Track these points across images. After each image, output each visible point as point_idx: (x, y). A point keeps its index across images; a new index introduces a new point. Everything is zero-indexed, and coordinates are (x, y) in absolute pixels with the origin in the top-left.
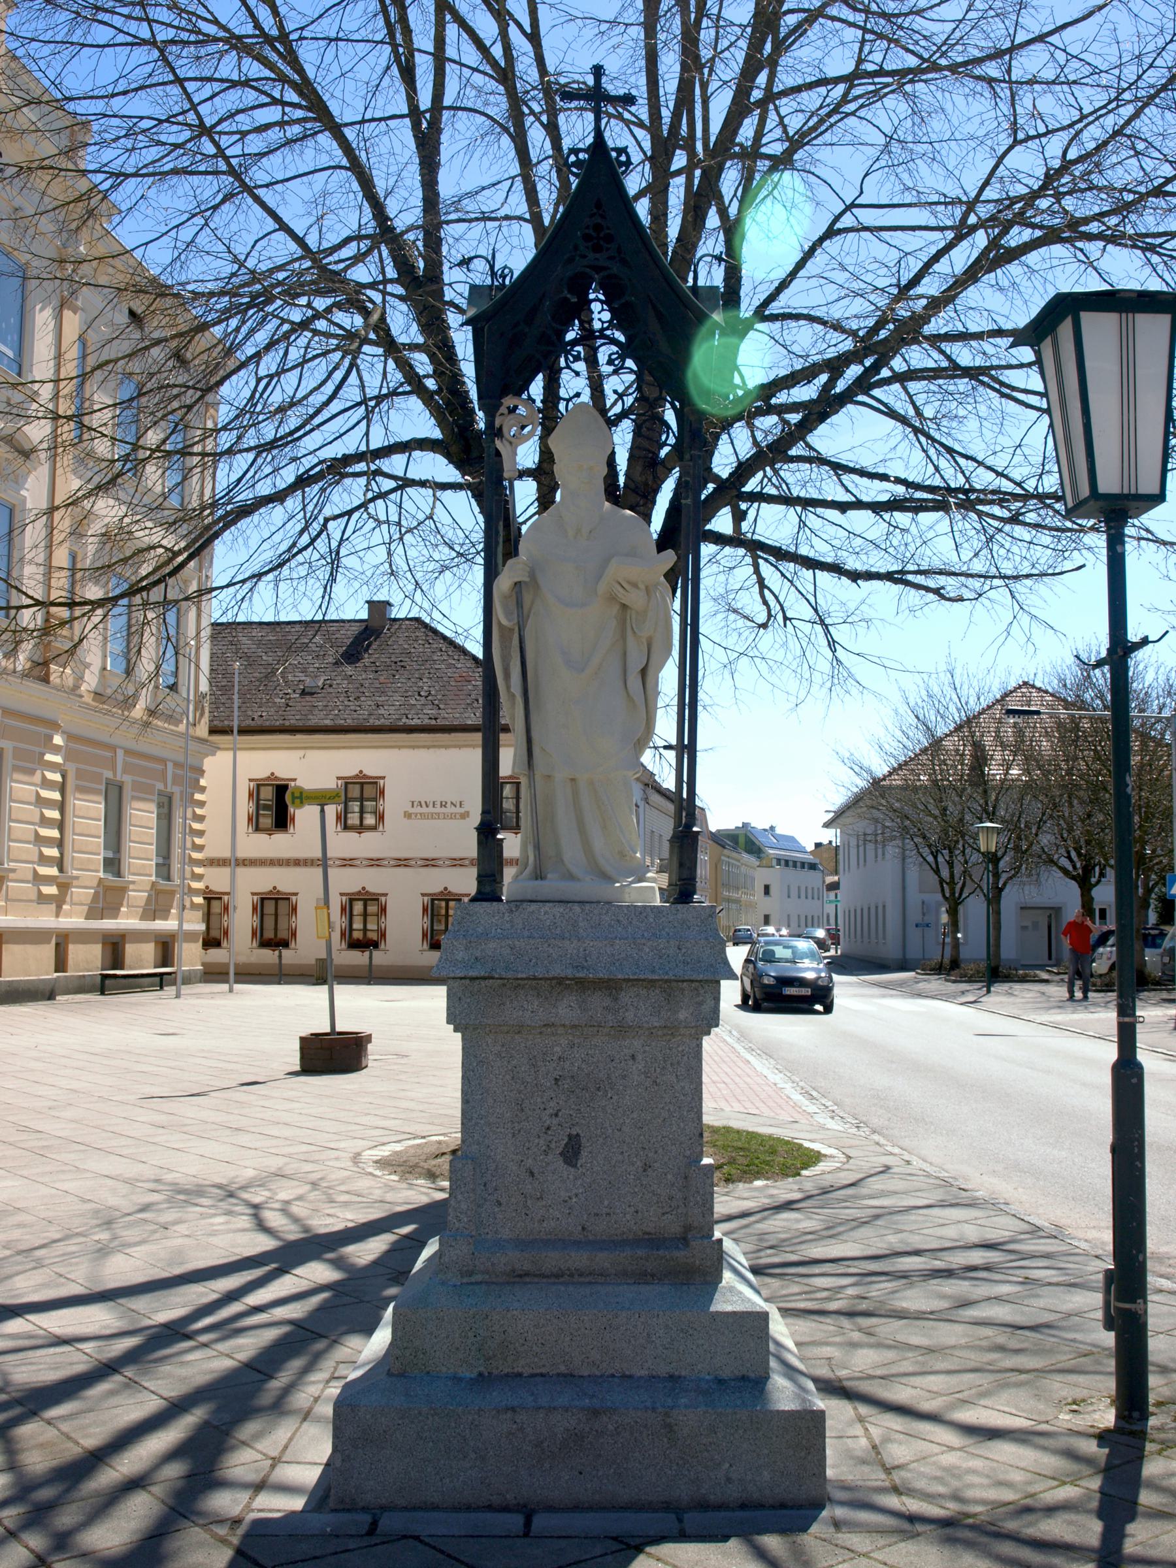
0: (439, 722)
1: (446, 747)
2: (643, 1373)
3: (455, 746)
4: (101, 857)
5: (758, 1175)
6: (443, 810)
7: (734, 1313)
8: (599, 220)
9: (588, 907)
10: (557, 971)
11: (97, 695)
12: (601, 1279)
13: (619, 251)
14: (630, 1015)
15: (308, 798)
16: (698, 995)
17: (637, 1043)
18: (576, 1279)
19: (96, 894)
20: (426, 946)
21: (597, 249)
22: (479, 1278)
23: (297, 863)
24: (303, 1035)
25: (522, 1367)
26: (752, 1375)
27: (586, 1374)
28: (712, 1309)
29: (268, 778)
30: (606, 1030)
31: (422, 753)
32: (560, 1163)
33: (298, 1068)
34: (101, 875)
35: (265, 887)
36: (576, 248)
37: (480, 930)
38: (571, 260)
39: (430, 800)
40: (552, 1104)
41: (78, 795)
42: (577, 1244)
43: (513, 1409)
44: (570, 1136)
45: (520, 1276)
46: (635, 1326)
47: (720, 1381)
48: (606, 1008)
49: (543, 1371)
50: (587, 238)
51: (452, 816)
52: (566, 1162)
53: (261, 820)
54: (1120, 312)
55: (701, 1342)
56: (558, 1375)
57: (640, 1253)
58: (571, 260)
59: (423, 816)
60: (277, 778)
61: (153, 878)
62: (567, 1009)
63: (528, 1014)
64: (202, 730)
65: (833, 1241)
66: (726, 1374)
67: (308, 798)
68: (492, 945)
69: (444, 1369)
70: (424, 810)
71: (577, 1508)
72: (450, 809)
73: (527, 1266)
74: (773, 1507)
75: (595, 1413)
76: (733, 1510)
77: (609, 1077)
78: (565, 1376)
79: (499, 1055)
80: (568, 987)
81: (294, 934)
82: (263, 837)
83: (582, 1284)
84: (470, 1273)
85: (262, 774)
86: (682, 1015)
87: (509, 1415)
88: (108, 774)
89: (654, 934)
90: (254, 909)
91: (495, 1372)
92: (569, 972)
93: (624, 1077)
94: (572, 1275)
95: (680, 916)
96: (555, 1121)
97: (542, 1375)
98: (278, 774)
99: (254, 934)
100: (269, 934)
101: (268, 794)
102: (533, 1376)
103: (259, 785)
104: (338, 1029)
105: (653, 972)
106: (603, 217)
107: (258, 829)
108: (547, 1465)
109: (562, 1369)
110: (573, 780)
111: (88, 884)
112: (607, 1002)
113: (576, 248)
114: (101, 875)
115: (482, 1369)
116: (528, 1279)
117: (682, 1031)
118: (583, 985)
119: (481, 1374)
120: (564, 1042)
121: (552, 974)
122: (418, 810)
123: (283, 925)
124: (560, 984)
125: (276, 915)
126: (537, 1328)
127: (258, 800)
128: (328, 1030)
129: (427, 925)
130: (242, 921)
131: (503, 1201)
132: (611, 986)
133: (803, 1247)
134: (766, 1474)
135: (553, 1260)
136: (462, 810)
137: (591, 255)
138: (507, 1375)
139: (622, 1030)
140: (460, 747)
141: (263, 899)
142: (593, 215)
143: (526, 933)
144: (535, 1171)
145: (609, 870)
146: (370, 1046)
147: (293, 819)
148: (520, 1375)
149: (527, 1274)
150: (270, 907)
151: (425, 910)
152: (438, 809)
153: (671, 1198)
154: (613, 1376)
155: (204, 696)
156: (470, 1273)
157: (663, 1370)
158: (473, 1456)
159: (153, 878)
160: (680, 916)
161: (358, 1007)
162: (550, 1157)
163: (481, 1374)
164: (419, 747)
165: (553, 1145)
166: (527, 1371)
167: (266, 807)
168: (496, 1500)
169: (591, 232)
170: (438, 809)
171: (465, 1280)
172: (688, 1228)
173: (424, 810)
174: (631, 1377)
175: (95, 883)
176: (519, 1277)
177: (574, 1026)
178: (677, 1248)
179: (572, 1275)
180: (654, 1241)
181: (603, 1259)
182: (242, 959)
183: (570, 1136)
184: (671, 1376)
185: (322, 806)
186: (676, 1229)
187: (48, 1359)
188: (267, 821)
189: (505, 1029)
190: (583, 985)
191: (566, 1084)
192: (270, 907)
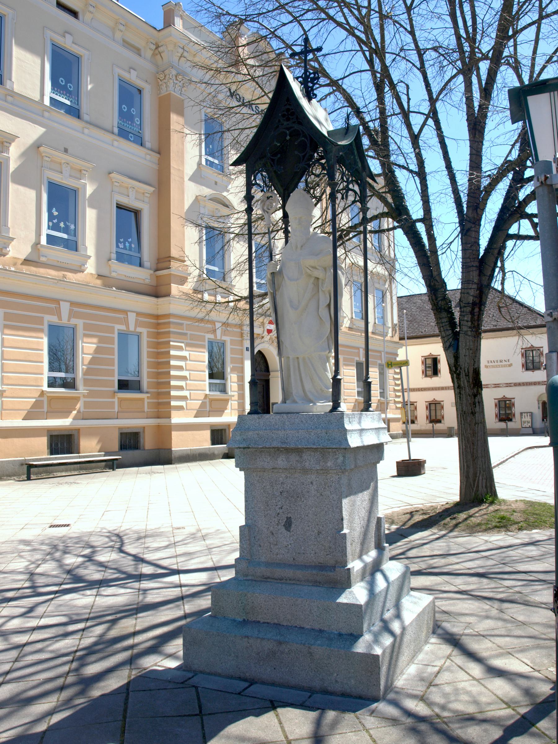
0: (497, 327)
1: (501, 337)
2: (308, 627)
3: (504, 337)
4: (356, 391)
5: (535, 527)
6: (501, 363)
7: (347, 604)
8: (288, 107)
9: (289, 415)
10: (275, 444)
11: (350, 328)
12: (298, 583)
13: (297, 118)
14: (307, 464)
15: (394, 364)
16: (336, 455)
17: (313, 477)
18: (288, 582)
19: (355, 405)
20: (497, 420)
21: (288, 119)
22: (250, 578)
23: (442, 388)
24: (398, 460)
25: (260, 618)
26: (355, 633)
27: (285, 624)
28: (338, 601)
29: (429, 355)
30: (299, 471)
31: (504, 339)
32: (283, 529)
33: (396, 474)
34: (357, 397)
35: (430, 399)
36: (279, 121)
37: (246, 427)
38: (277, 127)
39: (495, 360)
40: (280, 503)
41: (345, 367)
42: (290, 566)
43: (248, 637)
44: (287, 517)
45: (266, 578)
46: (305, 605)
47: (340, 635)
48: (297, 461)
49: (268, 621)
50: (283, 116)
51: (505, 366)
52: (286, 529)
53: (427, 372)
54: (550, 92)
55: (332, 616)
56: (274, 624)
57: (314, 572)
58: (277, 127)
59: (493, 367)
60: (432, 355)
61: (379, 398)
62: (281, 461)
63: (266, 463)
64: (396, 338)
65: (538, 562)
66: (344, 631)
67: (394, 364)
68: (250, 433)
69: (230, 616)
70: (493, 364)
71: (273, 684)
72: (504, 363)
73: (269, 575)
74: (356, 697)
75: (280, 643)
76: (338, 696)
77: (302, 492)
78: (277, 624)
79: (258, 481)
80: (281, 451)
81: (443, 417)
82: (428, 379)
83: (290, 584)
84: (247, 576)
85: (426, 354)
86: (329, 464)
87: (246, 639)
88: (357, 359)
89: (316, 427)
90: (427, 408)
91: (250, 619)
92: (279, 445)
93: (308, 492)
94: (286, 580)
95: (328, 418)
96: (281, 511)
97: (268, 623)
98: (432, 354)
99: (427, 418)
100: (433, 418)
101: (429, 362)
102: (264, 623)
103: (425, 359)
104: (412, 458)
105: (314, 444)
106: (290, 105)
107: (426, 376)
108: (261, 663)
109: (276, 621)
110: (298, 358)
111: (351, 401)
112: (298, 458)
113: (279, 121)
114: (357, 397)
115: (245, 617)
116: (269, 580)
117: (331, 471)
118: (288, 451)
119: (244, 620)
120: (283, 476)
121: (273, 446)
122: (491, 364)
123: (438, 413)
124: (278, 450)
125: (436, 410)
126: (267, 602)
127: (426, 364)
128: (408, 459)
129: (497, 411)
130: (422, 413)
131: (262, 545)
132: (298, 451)
133: (517, 565)
134: (353, 682)
135: (279, 572)
136: (509, 363)
137: (285, 123)
138: (254, 621)
139: (305, 471)
140: (506, 337)
141: (430, 404)
142: (285, 105)
143: (264, 428)
144: (274, 533)
145: (311, 397)
146: (426, 465)
147: (440, 371)
148: (259, 622)
149: (269, 578)
150: (433, 407)
151: (496, 405)
152: (499, 363)
153: (330, 548)
154: (296, 627)
155: (396, 325)
156: (247, 576)
157: (317, 627)
158: (233, 655)
159: (379, 398)
160: (328, 418)
161: (421, 448)
162: (280, 527)
163: (244, 620)
164: (489, 338)
165: (281, 521)
166: (262, 621)
167: (429, 367)
168: (242, 675)
169: (285, 113)
170: (499, 363)
171: (245, 578)
172: (337, 562)
173: (493, 364)
174: (303, 628)
175: (354, 401)
176: (266, 579)
177: (286, 469)
178: (331, 571)
179: (286, 580)
180: (322, 567)
181: (299, 574)
182: (423, 428)
183: (287, 517)
184: (320, 630)
185: (400, 368)
186: (332, 562)
187: (164, 593)
188: (430, 373)
189: (259, 470)
190: (288, 451)
191: (285, 494)
192: (433, 407)
